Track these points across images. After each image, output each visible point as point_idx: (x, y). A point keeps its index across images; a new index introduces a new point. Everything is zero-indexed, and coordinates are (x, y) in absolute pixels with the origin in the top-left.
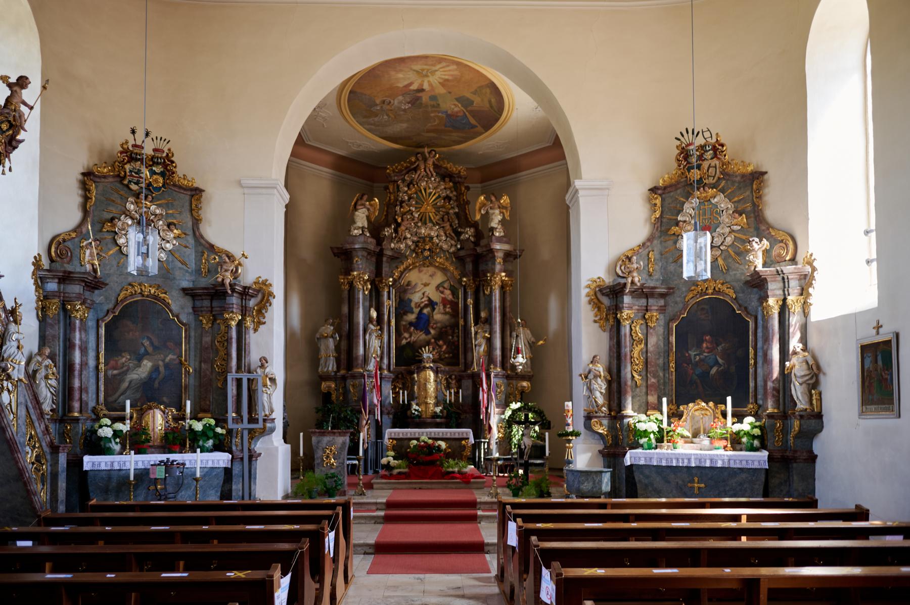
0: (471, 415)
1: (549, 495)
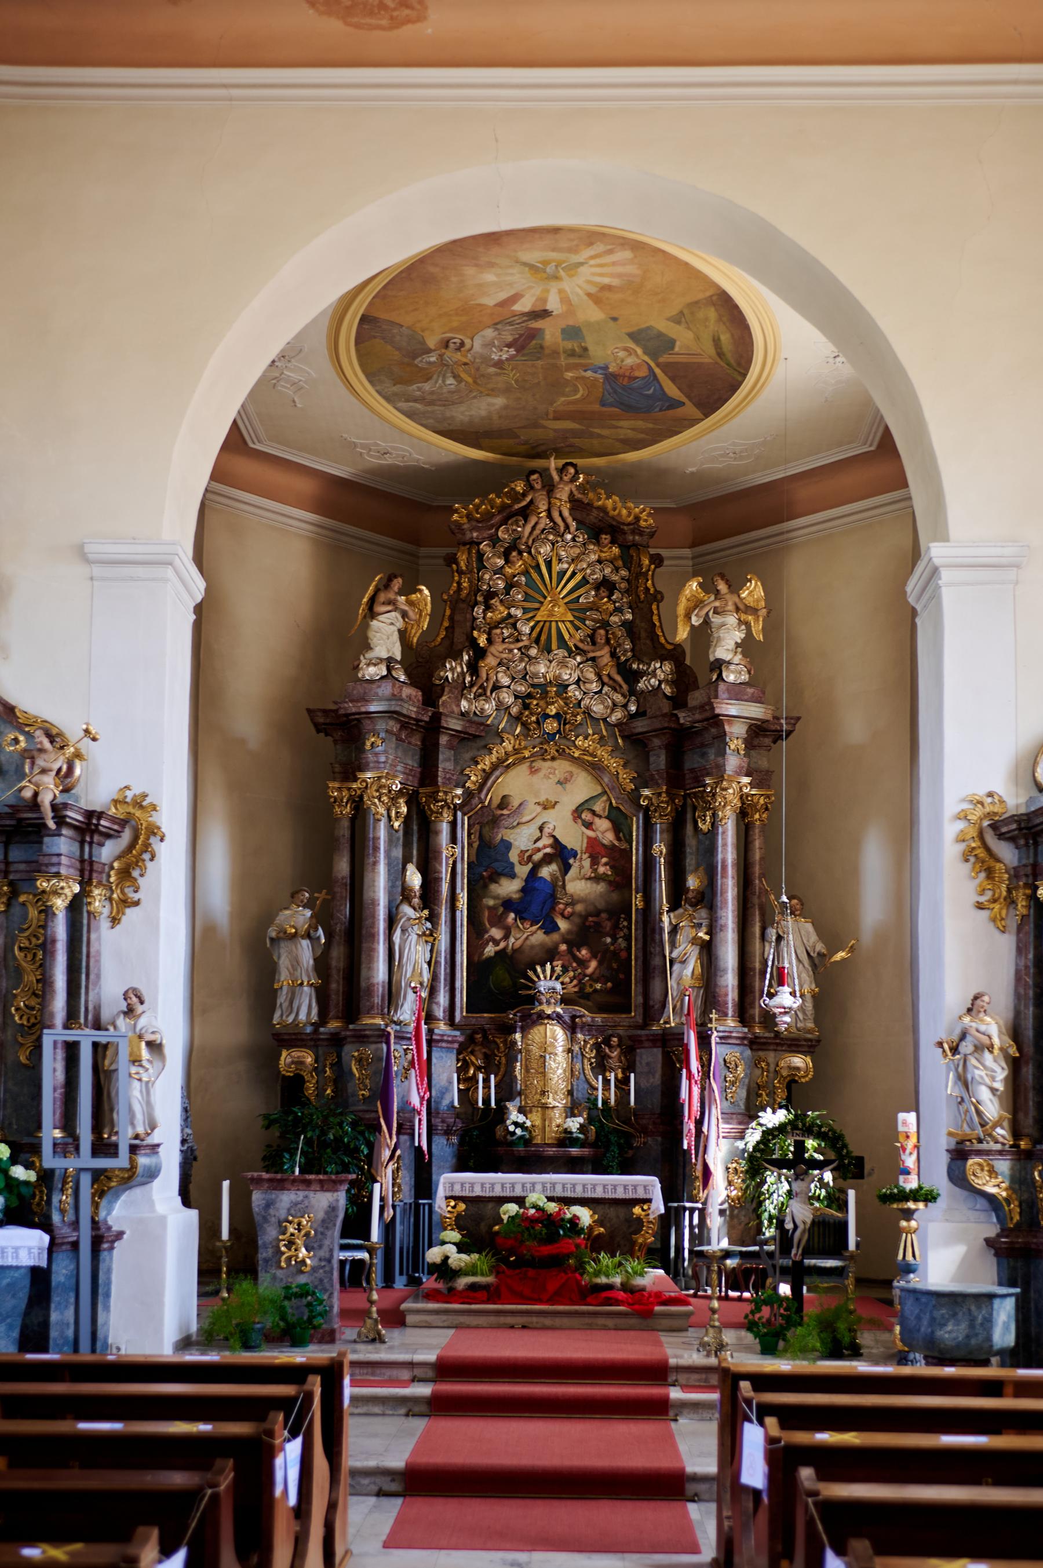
0: (659, 1139)
1: (855, 1352)
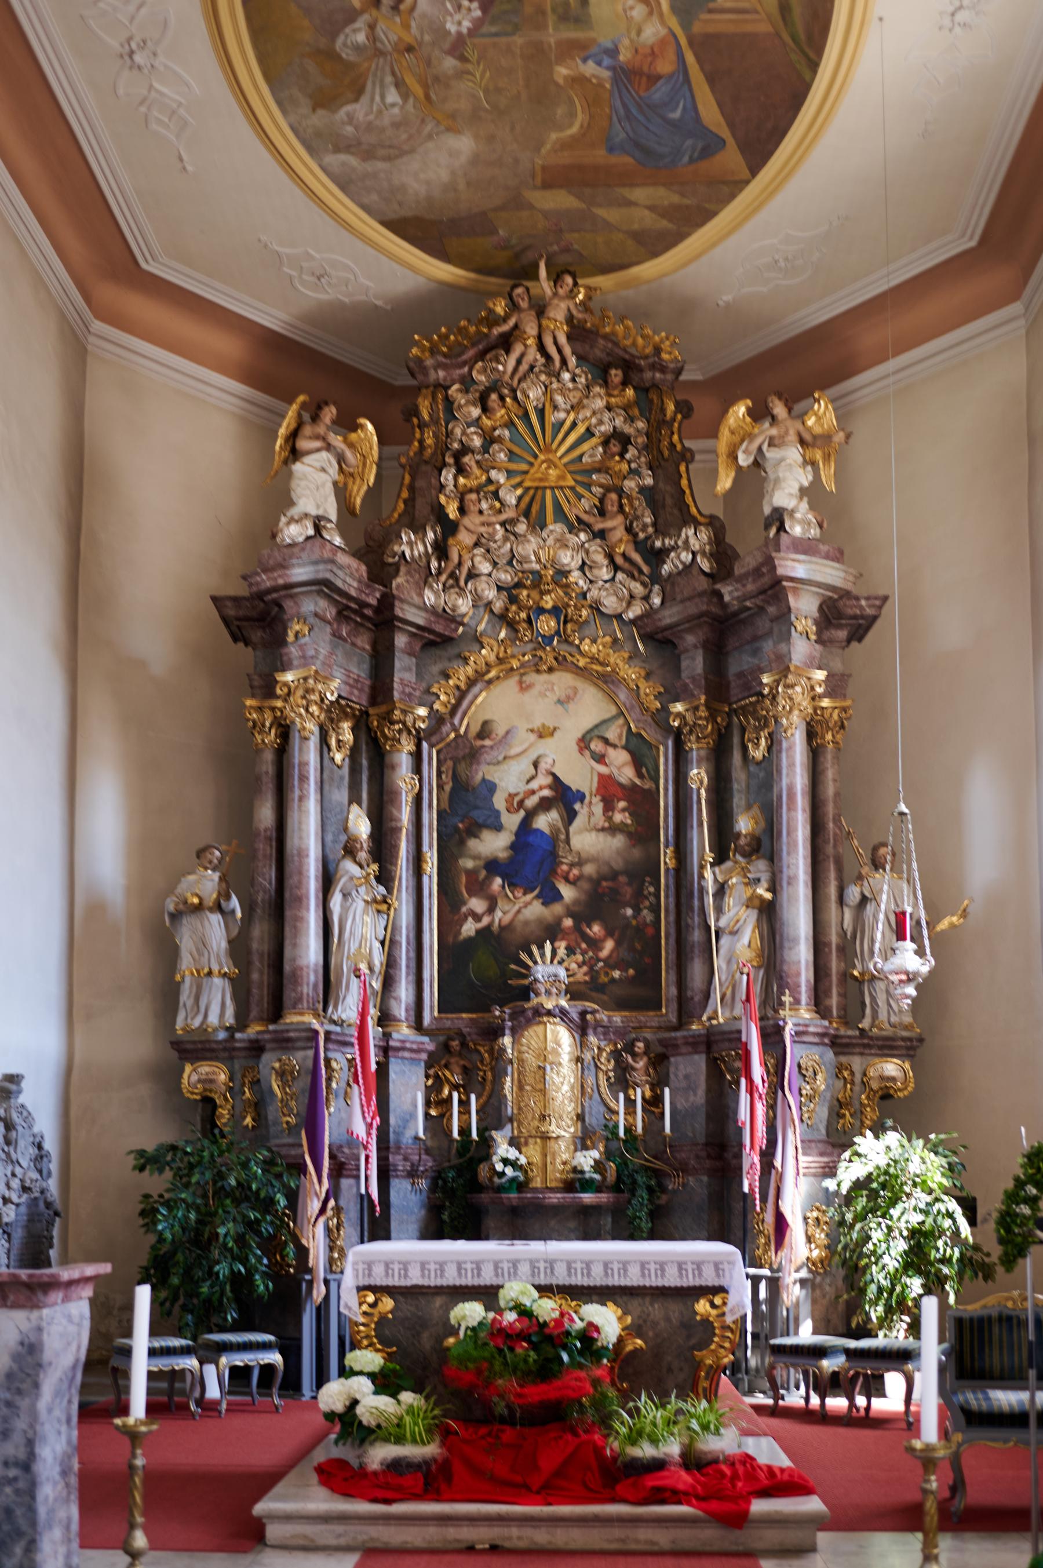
0: (705, 1179)
